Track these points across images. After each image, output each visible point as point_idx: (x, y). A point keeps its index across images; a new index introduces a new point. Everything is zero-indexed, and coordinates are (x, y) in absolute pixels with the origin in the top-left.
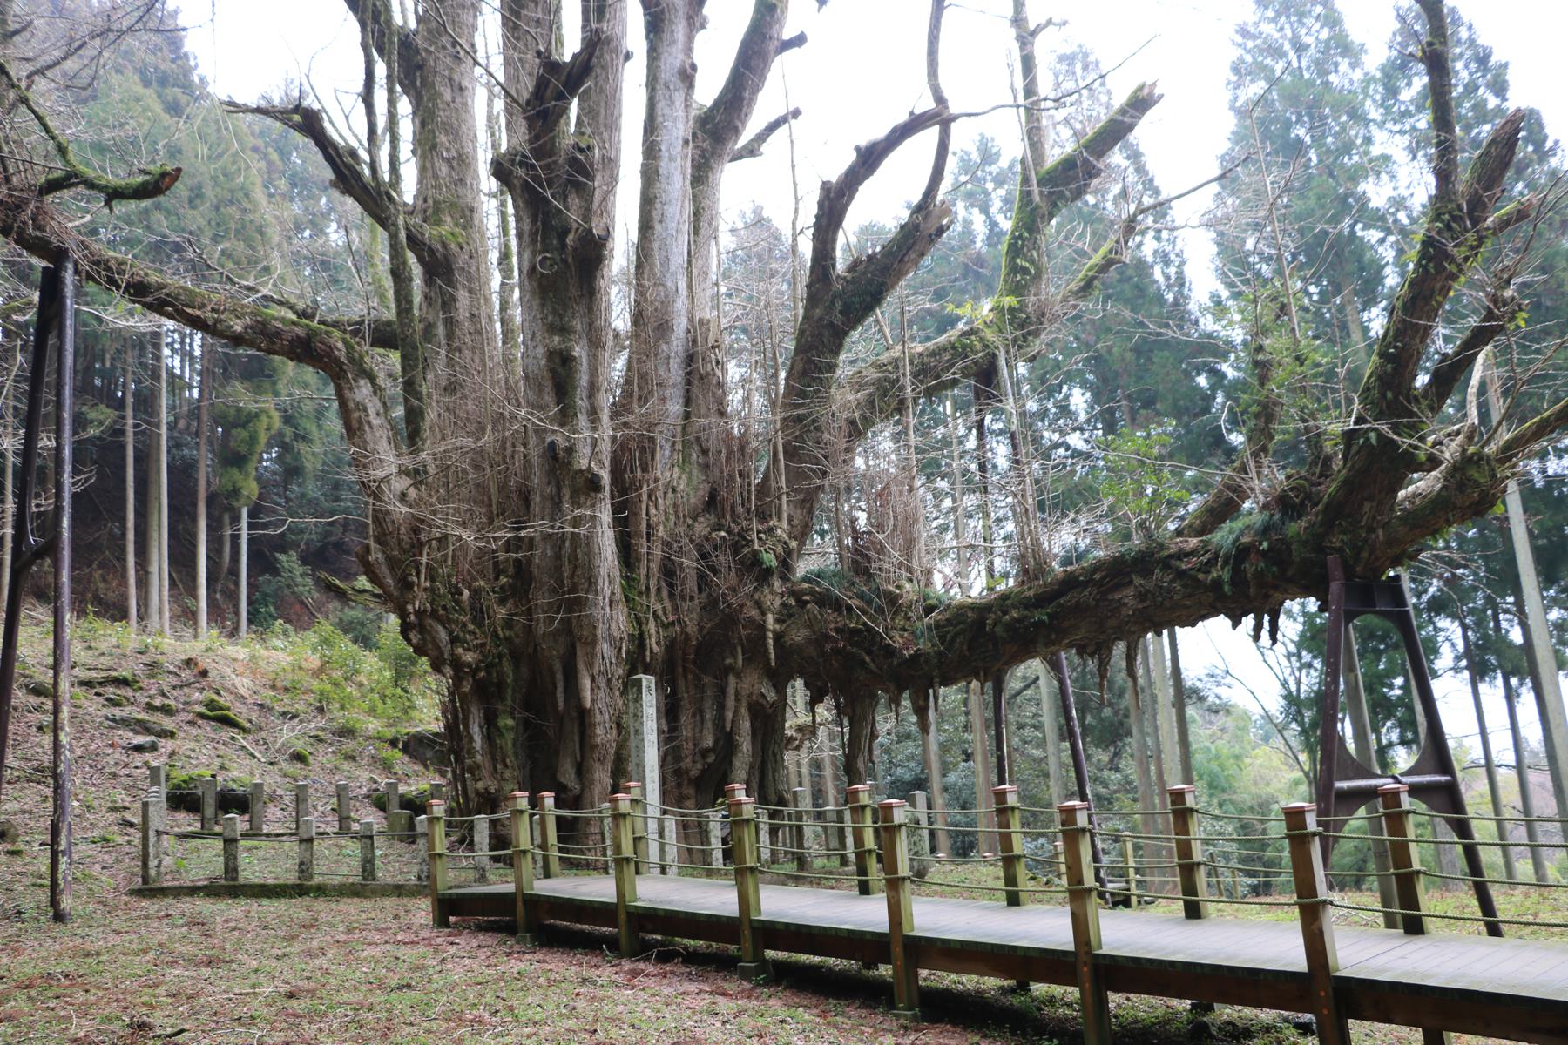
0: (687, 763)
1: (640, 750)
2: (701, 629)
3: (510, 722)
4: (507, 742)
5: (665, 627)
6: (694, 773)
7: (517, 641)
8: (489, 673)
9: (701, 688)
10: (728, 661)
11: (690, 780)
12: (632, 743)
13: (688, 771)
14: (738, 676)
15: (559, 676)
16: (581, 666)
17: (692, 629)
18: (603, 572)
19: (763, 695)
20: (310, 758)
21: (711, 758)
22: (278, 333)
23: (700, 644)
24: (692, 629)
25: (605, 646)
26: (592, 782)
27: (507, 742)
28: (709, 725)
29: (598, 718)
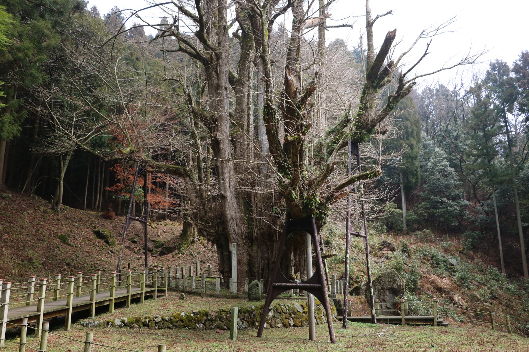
18: (229, 217)
22: (171, 170)
25: (234, 236)
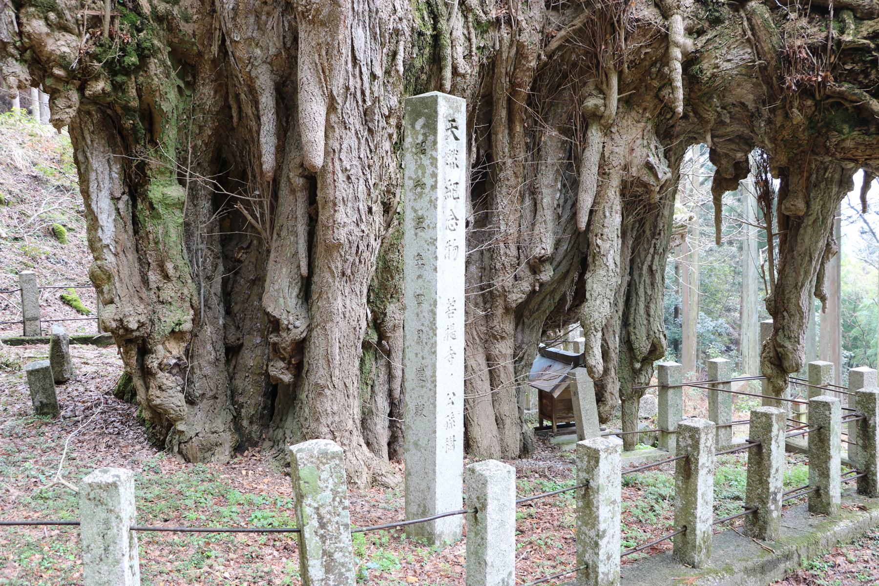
0: (503, 280)
1: (426, 262)
2: (547, 39)
3: (176, 192)
4: (168, 229)
5: (482, 28)
6: (516, 297)
7: (187, 28)
8: (118, 87)
9: (535, 148)
10: (591, 103)
11: (507, 310)
12: (410, 245)
13: (505, 293)
14: (607, 130)
15: (267, 100)
16: (306, 74)
17: (530, 38)
19: (650, 167)
20: (67, 235)
21: (547, 274)
23: (541, 72)
24: (530, 38)
25: (361, 37)
26: (329, 317)
27: (168, 229)
28: (547, 214)
29: (342, 189)
